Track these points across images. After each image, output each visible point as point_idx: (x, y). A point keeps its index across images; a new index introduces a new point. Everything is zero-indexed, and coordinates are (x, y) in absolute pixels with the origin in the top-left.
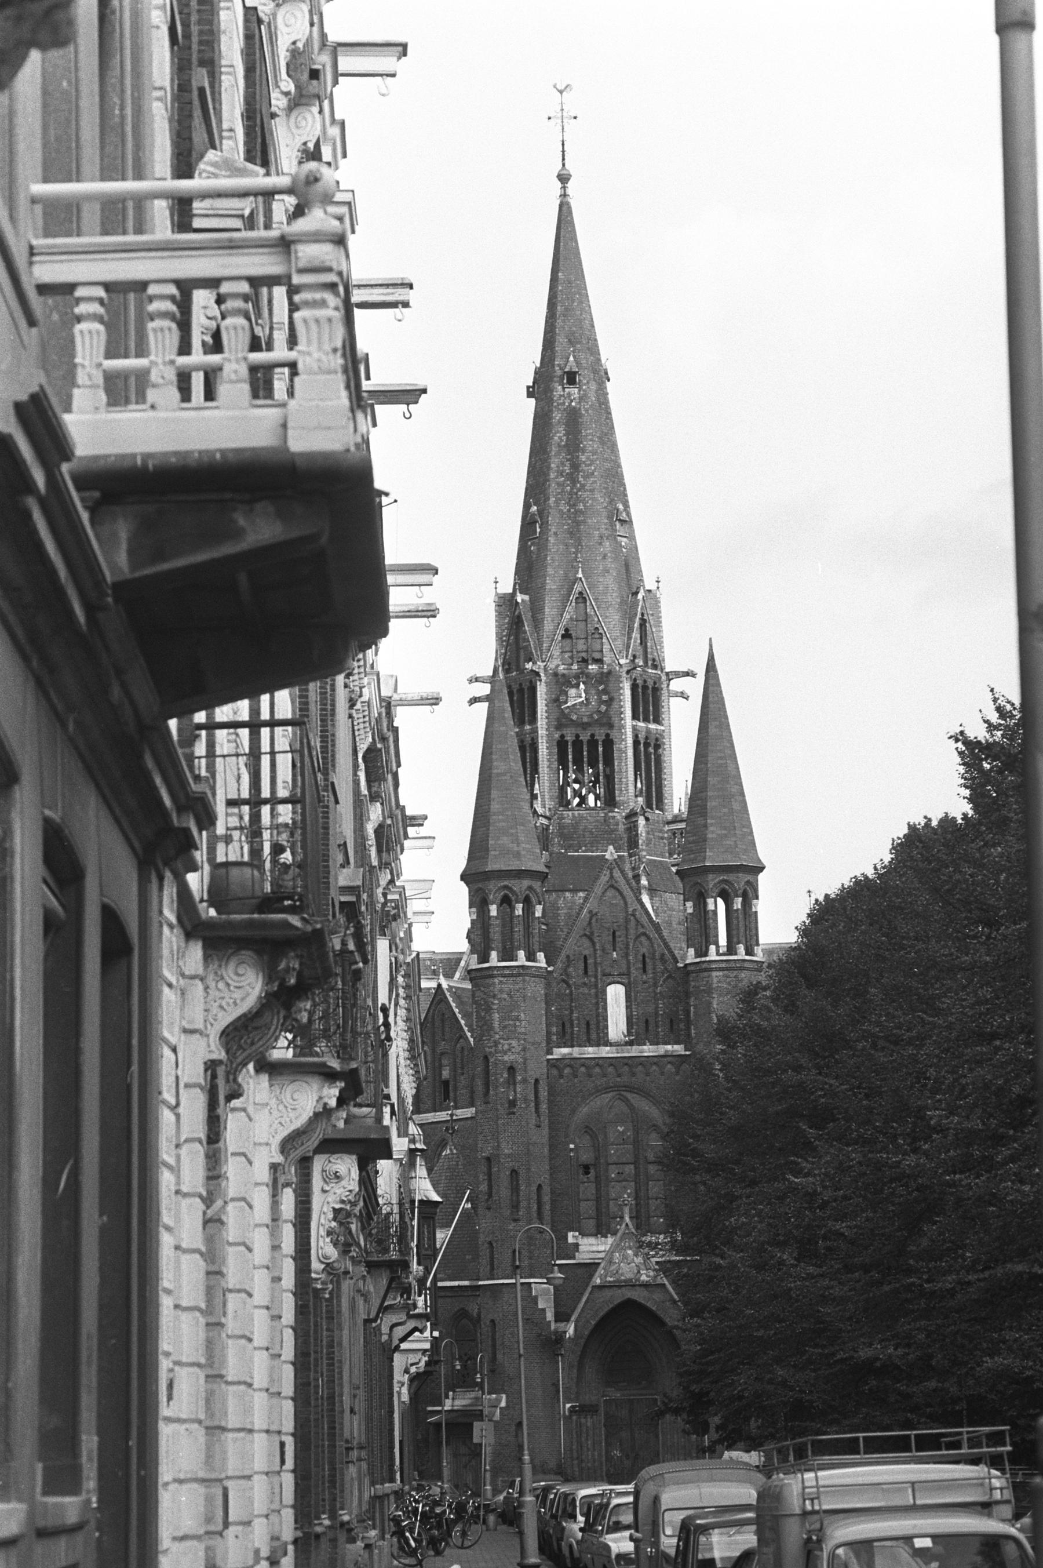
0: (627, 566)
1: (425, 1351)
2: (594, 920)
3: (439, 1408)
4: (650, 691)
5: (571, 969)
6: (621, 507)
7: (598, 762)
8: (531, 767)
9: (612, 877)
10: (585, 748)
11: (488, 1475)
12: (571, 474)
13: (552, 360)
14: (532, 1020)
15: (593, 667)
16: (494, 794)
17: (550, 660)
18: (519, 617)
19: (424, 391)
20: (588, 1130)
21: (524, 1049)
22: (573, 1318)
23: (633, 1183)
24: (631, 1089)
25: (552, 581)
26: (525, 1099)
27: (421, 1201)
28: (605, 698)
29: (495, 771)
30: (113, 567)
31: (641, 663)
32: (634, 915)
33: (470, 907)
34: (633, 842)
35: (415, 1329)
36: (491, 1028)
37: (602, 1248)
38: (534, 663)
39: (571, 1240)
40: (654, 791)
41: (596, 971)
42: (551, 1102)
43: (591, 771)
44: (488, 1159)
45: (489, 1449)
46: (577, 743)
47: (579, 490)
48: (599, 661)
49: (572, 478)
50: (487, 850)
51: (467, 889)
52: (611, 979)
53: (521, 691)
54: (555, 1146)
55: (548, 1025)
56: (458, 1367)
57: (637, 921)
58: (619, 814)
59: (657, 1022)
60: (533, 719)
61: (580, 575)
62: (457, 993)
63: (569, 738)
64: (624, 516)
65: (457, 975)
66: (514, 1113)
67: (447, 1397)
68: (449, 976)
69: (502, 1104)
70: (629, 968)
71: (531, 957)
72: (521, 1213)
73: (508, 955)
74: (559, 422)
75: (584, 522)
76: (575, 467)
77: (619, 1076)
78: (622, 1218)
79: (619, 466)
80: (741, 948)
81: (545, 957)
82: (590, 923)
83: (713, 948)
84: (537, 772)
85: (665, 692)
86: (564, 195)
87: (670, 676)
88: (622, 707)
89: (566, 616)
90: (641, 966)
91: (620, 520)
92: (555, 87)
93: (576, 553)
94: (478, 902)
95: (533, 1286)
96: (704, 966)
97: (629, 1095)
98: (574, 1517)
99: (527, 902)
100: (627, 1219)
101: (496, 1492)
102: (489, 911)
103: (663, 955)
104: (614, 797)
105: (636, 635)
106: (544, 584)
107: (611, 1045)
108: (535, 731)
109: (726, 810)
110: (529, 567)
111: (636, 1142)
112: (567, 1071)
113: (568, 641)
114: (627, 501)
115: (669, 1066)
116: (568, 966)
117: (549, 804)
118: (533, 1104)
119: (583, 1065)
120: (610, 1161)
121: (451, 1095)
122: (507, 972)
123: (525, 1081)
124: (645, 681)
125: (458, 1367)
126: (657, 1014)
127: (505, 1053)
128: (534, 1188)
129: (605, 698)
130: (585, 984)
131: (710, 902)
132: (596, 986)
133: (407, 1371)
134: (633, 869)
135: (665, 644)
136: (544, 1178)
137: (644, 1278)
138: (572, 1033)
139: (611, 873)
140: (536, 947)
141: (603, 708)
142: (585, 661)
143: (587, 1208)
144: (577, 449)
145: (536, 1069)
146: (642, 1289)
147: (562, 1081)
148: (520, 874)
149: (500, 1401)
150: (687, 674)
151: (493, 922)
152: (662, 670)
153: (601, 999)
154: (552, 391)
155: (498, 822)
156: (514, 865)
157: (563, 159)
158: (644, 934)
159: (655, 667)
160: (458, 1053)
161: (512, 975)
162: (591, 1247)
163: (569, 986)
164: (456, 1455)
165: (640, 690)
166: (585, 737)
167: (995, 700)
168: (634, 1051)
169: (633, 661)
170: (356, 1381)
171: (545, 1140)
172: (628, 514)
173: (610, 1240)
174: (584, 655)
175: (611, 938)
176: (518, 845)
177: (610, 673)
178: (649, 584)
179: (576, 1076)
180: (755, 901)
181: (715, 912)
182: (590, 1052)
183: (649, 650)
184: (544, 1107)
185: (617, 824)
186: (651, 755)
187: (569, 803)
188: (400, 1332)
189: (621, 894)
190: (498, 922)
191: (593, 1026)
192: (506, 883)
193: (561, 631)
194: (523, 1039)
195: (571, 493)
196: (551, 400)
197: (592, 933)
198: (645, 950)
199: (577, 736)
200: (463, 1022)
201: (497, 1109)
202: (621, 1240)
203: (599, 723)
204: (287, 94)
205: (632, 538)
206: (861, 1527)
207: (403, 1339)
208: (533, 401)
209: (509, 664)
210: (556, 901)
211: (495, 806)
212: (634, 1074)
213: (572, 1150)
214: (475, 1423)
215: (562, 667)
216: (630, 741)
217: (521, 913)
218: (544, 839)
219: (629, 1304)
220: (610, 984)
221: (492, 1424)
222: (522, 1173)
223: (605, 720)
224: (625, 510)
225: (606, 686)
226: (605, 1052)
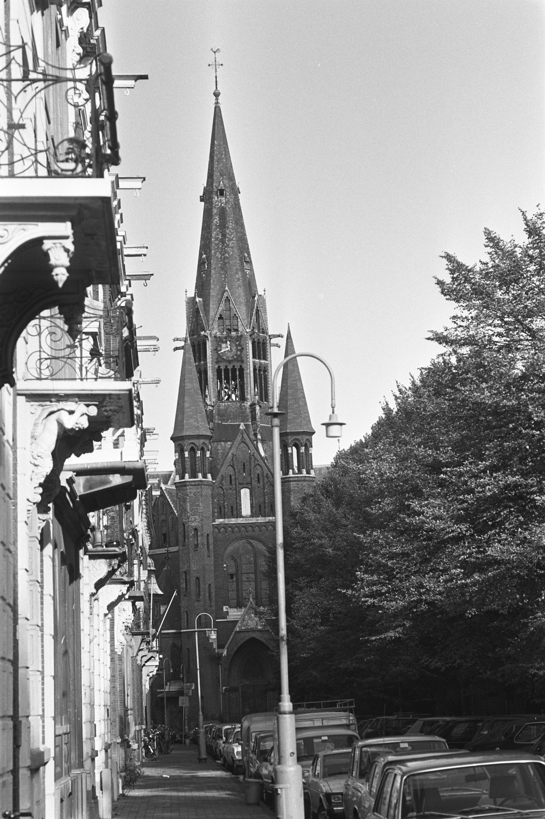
0: (249, 284)
1: (156, 666)
2: (234, 458)
3: (163, 690)
4: (261, 344)
5: (224, 482)
6: (246, 255)
7: (236, 379)
8: (203, 382)
9: (243, 437)
10: (230, 372)
11: (186, 721)
12: (222, 239)
13: (212, 184)
14: (205, 507)
15: (234, 333)
16: (186, 399)
17: (214, 330)
18: (198, 309)
19: (152, 275)
20: (233, 558)
21: (201, 520)
22: (226, 647)
23: (253, 583)
24: (253, 538)
25: (214, 292)
26: (203, 544)
27: (154, 594)
28: (239, 348)
29: (186, 388)
30: (79, 491)
31: (257, 331)
32: (253, 455)
33: (175, 452)
34: (254, 418)
35: (152, 657)
36: (186, 510)
37: (239, 613)
38: (205, 331)
39: (225, 610)
40: (264, 394)
41: (236, 482)
42: (215, 545)
43: (233, 383)
44: (185, 572)
45: (187, 709)
46: (226, 370)
47: (226, 247)
48: (236, 330)
49: (223, 241)
50: (183, 426)
51: (173, 444)
52: (243, 486)
53: (199, 345)
54: (217, 566)
55: (213, 508)
56: (172, 671)
57: (255, 458)
58: (248, 404)
59: (265, 506)
61: (227, 289)
62: (169, 491)
63: (222, 368)
64: (248, 259)
65: (170, 483)
66: (197, 550)
67: (166, 685)
68: (166, 483)
70: (251, 481)
71: (205, 476)
72: (201, 598)
73: (194, 475)
74: (216, 214)
75: (229, 263)
76: (224, 236)
77: (247, 532)
78: (249, 599)
79: (245, 235)
80: (304, 471)
81: (211, 476)
82: (232, 459)
83: (291, 471)
84: (207, 384)
85: (268, 345)
86: (217, 103)
87: (271, 337)
88: (247, 352)
89: (220, 308)
90: (257, 480)
91: (246, 262)
92: (212, 50)
93: (225, 278)
94: (180, 450)
97: (251, 541)
98: (222, 738)
99: (202, 449)
100: (251, 600)
101: (190, 729)
102: (184, 455)
103: (267, 474)
104: (245, 396)
105: (254, 317)
106: (210, 293)
107: (243, 517)
108: (206, 364)
109: (297, 406)
110: (202, 286)
111: (256, 563)
113: (221, 321)
114: (249, 252)
115: (271, 527)
116: (222, 480)
117: (213, 400)
118: (206, 546)
120: (243, 572)
121: (167, 540)
122: (193, 483)
123: (202, 535)
124: (259, 340)
125: (172, 671)
126: (265, 502)
127: (193, 522)
128: (207, 586)
129: (239, 348)
130: (231, 489)
131: (290, 449)
132: (236, 489)
133: (148, 675)
134: (254, 430)
135: (268, 321)
136: (212, 581)
137: (259, 627)
138: (225, 512)
139: (242, 436)
140: (207, 471)
141: (239, 353)
142: (230, 330)
143: (232, 595)
145: (208, 529)
147: (220, 534)
148: (199, 437)
149: (192, 686)
150: (279, 336)
151: (187, 459)
152: (267, 334)
154: (212, 199)
155: (188, 411)
156: (197, 433)
157: (216, 85)
158: (259, 464)
159: (263, 333)
161: (195, 485)
162: (234, 614)
163: (223, 489)
165: (256, 344)
166: (230, 367)
167: (398, 386)
168: (254, 520)
169: (253, 330)
170: (129, 683)
171: (212, 563)
172: (250, 258)
173: (243, 610)
174: (229, 327)
175: (242, 467)
176: (198, 423)
177: (241, 336)
178: (260, 292)
179: (226, 532)
180: (310, 448)
181: (292, 454)
182: (233, 521)
183: (261, 325)
184: (211, 547)
185: (246, 409)
186: (262, 375)
187: (223, 399)
188: (145, 659)
189: (247, 445)
190: (189, 460)
191: (234, 509)
192: (192, 441)
194: (200, 517)
195: (222, 248)
196: (211, 203)
197: (234, 464)
198: (259, 472)
199: (226, 367)
200: (172, 506)
201: (189, 549)
202: (248, 610)
203: (237, 360)
204: (79, 54)
205: (252, 270)
206: (308, 733)
207: (146, 662)
208: (203, 203)
209: (193, 332)
210: (217, 447)
211: (187, 405)
212: (254, 531)
214: (180, 697)
215: (218, 333)
216: (252, 369)
217: (199, 455)
218: (210, 417)
219: (253, 640)
220: (242, 488)
221: (188, 698)
222: (201, 579)
223: (239, 359)
224: (248, 256)
225: (240, 342)
226: (240, 521)
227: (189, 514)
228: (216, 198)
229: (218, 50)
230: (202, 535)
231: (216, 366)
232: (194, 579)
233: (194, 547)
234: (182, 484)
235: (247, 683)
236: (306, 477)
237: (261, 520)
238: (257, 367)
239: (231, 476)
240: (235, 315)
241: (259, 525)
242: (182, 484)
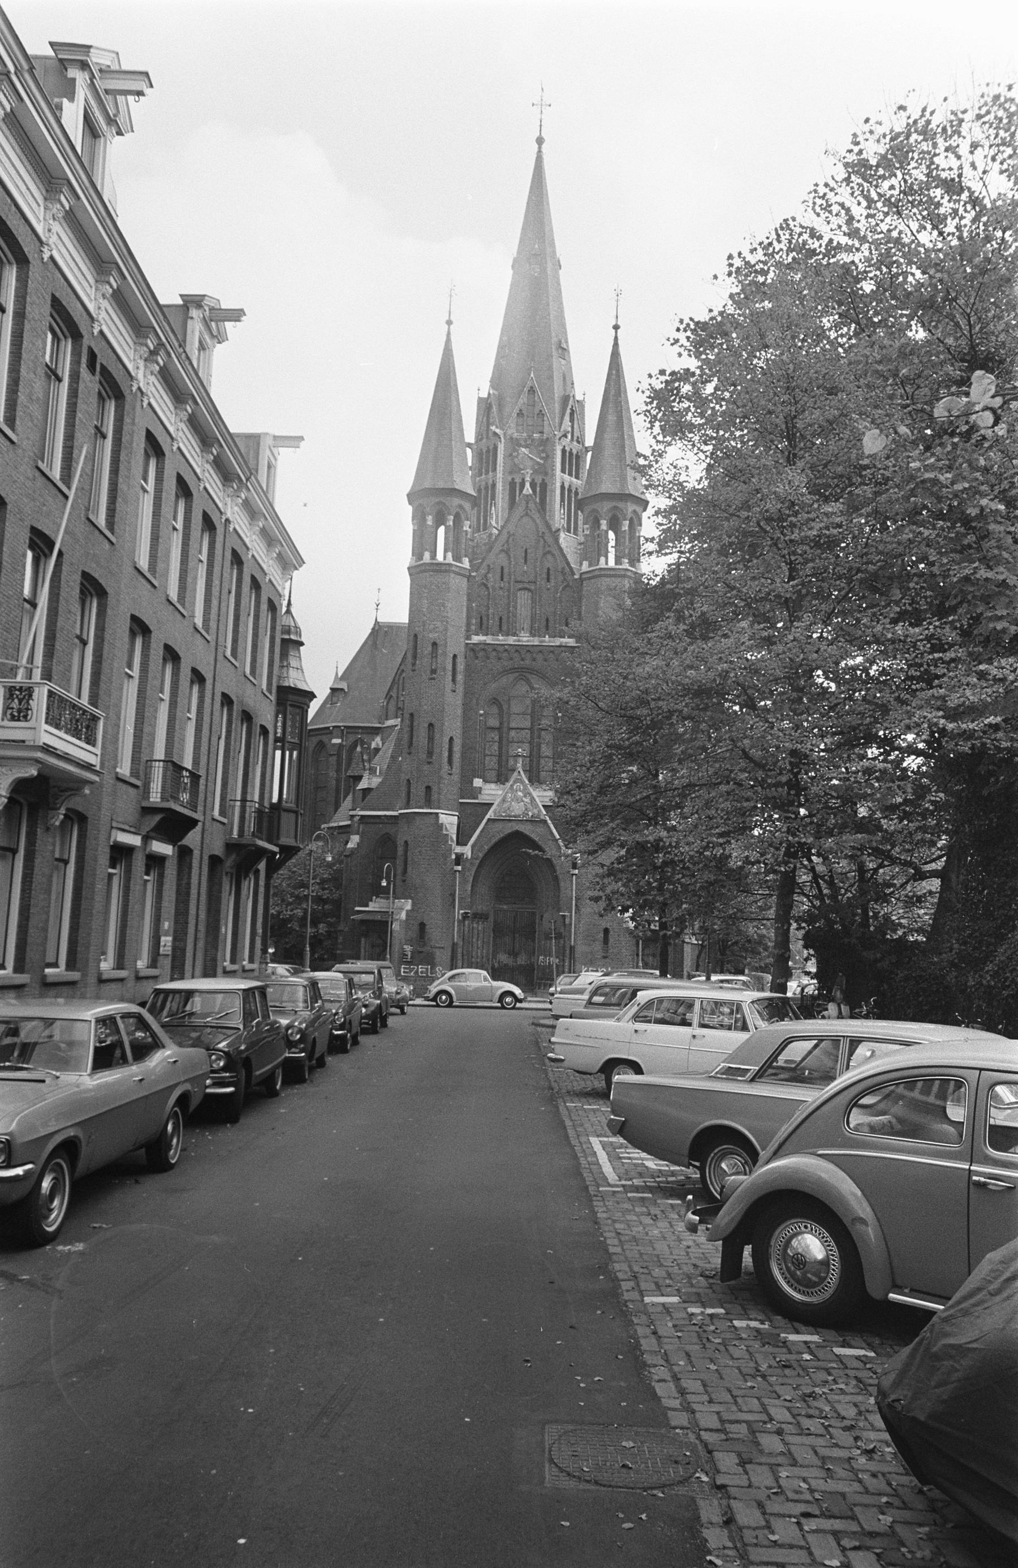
5: (490, 575)
20: (495, 701)
53: (488, 451)
60: (495, 470)
69: (425, 672)
83: (602, 559)
86: (540, 151)
89: (521, 401)
95: (441, 816)
96: (597, 573)
112: (481, 654)
119: (494, 650)
129: (543, 455)
143: (491, 762)
158: (549, 552)
171: (459, 702)
184: (460, 677)
189: (534, 521)
193: (516, 411)
197: (509, 549)
213: (481, 715)
219: (517, 835)
230: (445, 654)
231: (510, 479)
232: (426, 725)
233: (428, 672)
236: (627, 570)
238: (567, 486)
239: (502, 568)
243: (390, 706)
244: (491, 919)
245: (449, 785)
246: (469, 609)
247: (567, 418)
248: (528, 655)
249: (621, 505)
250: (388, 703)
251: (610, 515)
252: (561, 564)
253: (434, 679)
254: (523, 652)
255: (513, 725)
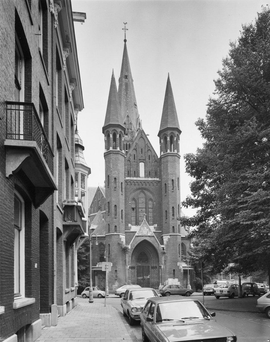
2: (137, 145)
5: (131, 157)
9: (142, 135)
16: (112, 105)
20: (134, 199)
22: (130, 244)
28: (132, 136)
44: (109, 203)
46: (127, 145)
48: (131, 129)
49: (126, 95)
55: (125, 171)
76: (127, 93)
82: (136, 146)
92: (124, 23)
95: (120, 235)
97: (144, 191)
112: (129, 183)
113: (125, 125)
115: (155, 183)
118: (121, 188)
126: (152, 170)
129: (132, 136)
141: (132, 138)
143: (133, 219)
144: (127, 90)
146: (149, 237)
153: (138, 166)
158: (150, 150)
160: (102, 200)
164: (99, 278)
166: (128, 144)
177: (133, 131)
182: (135, 179)
184: (123, 190)
192: (115, 128)
199: (127, 143)
211: (112, 109)
213: (130, 203)
219: (145, 241)
227: (112, 170)
228: (124, 79)
229: (126, 23)
230: (119, 182)
234: (109, 153)
235: (140, 265)
237: (150, 179)
239: (134, 155)
240: (131, 123)
241: (148, 182)
242: (109, 153)
243: (92, 210)
244: (136, 268)
245: (122, 227)
246: (125, 168)
247: (138, 125)
248: (144, 184)
249: (174, 132)
250: (91, 209)
251: (170, 135)
252: (153, 154)
253: (116, 190)
254: (143, 183)
255: (140, 207)
